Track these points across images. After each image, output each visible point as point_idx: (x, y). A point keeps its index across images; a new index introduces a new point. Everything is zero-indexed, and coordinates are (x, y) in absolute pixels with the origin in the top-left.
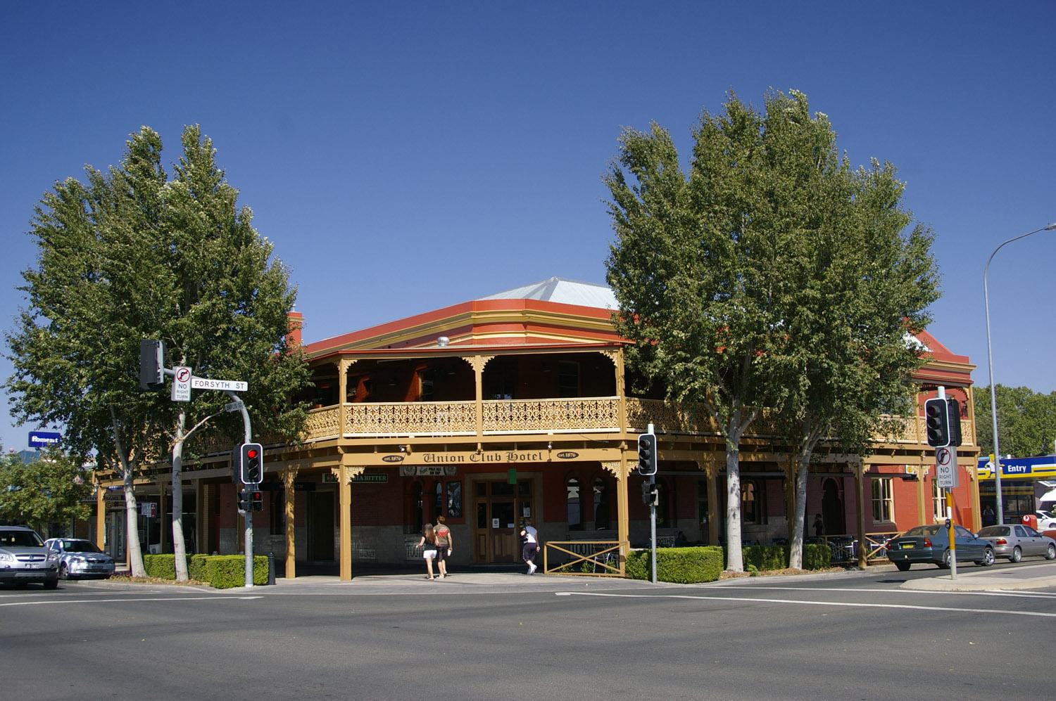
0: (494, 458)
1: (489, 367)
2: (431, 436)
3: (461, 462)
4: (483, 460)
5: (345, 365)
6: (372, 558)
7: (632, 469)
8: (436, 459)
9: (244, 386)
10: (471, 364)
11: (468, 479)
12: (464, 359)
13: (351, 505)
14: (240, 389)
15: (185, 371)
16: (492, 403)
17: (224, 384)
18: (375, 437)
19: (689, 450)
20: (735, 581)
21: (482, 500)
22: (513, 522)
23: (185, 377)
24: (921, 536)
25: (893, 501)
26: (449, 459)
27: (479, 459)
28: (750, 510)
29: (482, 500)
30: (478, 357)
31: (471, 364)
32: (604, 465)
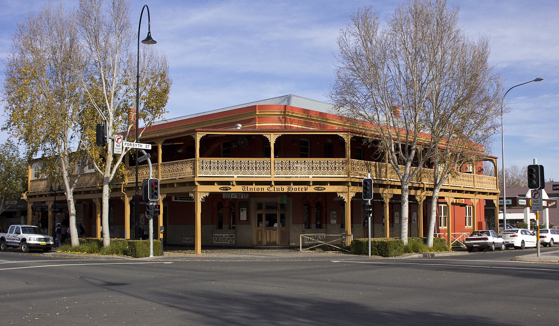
0: (280, 189)
1: (278, 140)
2: (298, 177)
3: (262, 191)
4: (274, 190)
5: (199, 137)
6: (191, 242)
7: (352, 197)
8: (249, 189)
11: (253, 201)
12: (264, 135)
13: (130, 215)
14: (148, 148)
15: (119, 137)
16: (279, 160)
18: (253, 177)
19: (377, 187)
20: (412, 256)
21: (260, 212)
22: (277, 223)
23: (120, 141)
25: (472, 217)
26: (256, 189)
27: (272, 190)
29: (260, 212)
30: (272, 134)
32: (338, 195)
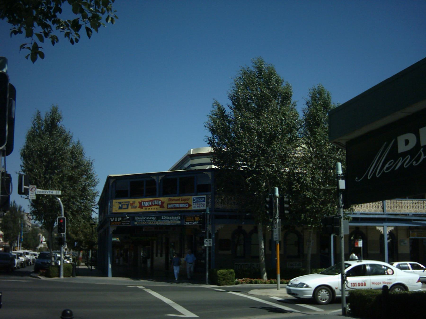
9: (60, 193)
10: (380, 230)
15: (33, 187)
17: (50, 192)
24: (206, 198)
28: (379, 267)
31: (380, 230)
